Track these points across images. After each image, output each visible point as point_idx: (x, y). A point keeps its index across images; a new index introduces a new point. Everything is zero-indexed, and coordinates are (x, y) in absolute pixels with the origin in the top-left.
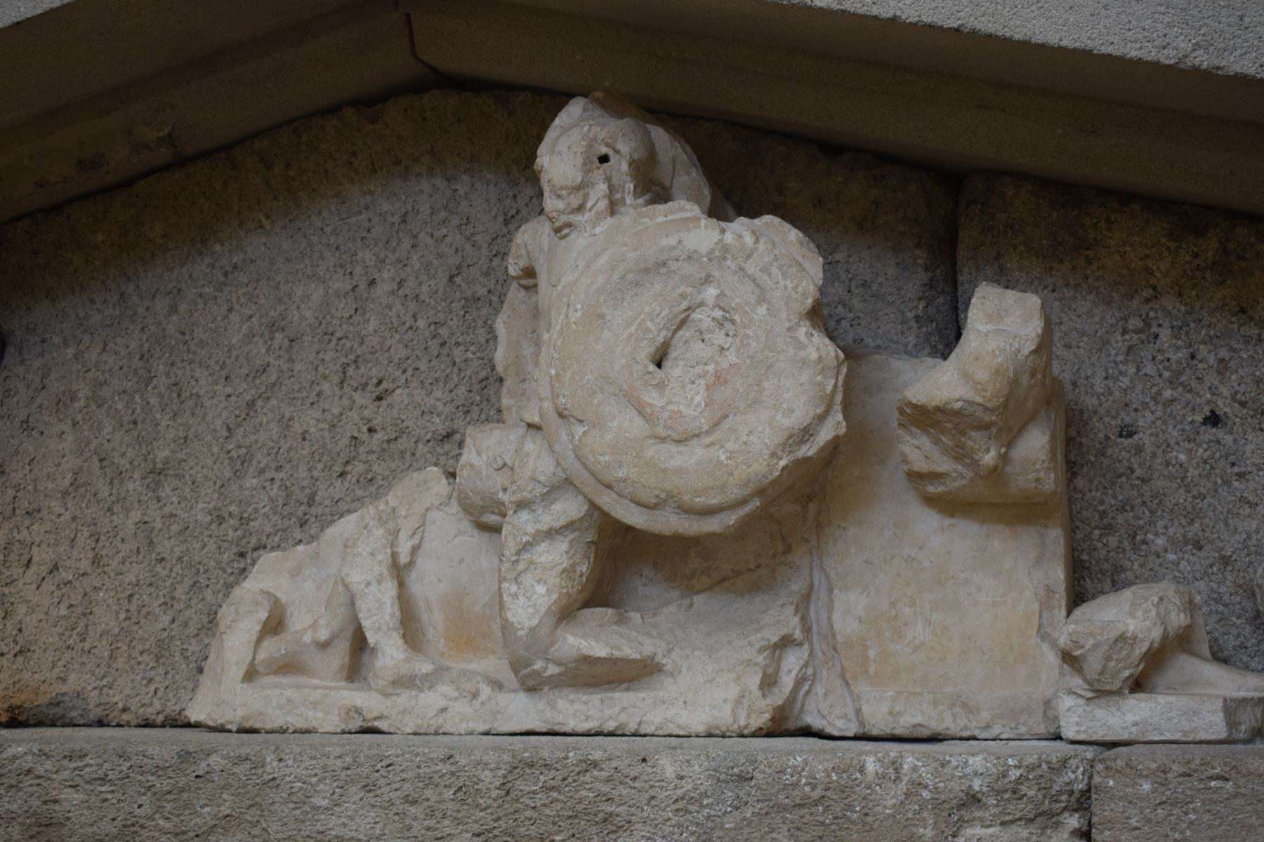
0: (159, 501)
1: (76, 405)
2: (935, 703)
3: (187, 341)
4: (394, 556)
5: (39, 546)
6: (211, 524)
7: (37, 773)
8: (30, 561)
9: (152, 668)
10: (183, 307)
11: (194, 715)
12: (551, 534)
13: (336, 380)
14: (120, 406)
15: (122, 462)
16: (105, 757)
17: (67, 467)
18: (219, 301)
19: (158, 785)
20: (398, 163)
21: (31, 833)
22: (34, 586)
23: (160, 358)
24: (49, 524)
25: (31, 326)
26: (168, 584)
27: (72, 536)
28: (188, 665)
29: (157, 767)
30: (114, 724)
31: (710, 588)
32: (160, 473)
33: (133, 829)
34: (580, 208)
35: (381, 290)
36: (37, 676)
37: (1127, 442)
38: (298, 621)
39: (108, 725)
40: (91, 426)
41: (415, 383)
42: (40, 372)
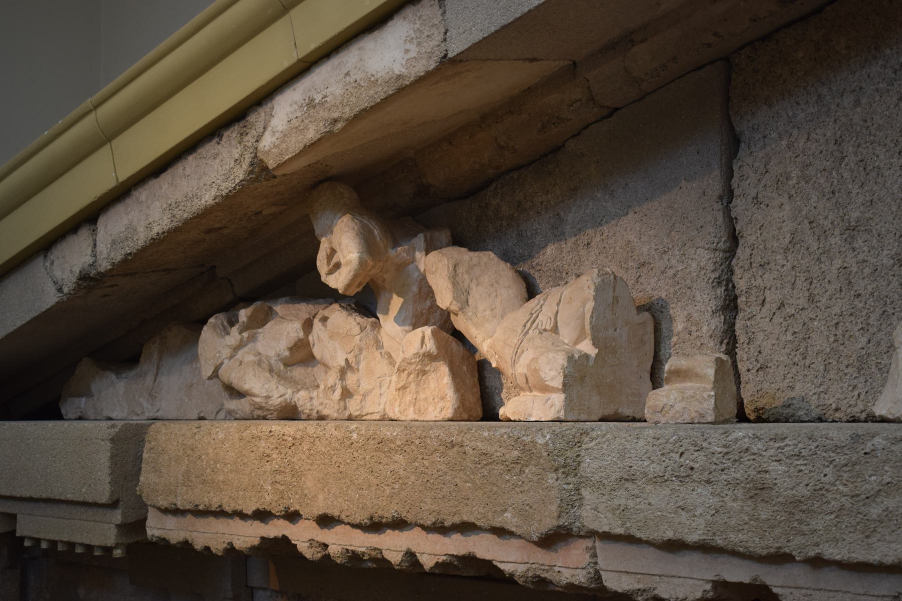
0: (854, 251)
1: (790, 183)
3: (868, 127)
5: (770, 289)
6: (893, 266)
7: (752, 451)
8: (764, 301)
9: (856, 377)
10: (864, 101)
11: (880, 410)
14: (822, 181)
15: (826, 223)
16: (799, 439)
17: (786, 229)
18: (891, 93)
19: (837, 460)
21: (751, 494)
22: (768, 319)
23: (849, 142)
24: (776, 273)
25: (756, 127)
26: (864, 313)
27: (793, 280)
28: (882, 375)
29: (836, 446)
30: (830, 420)
32: (853, 230)
33: (821, 492)
36: (773, 385)
39: (826, 421)
40: (802, 197)
42: (764, 160)
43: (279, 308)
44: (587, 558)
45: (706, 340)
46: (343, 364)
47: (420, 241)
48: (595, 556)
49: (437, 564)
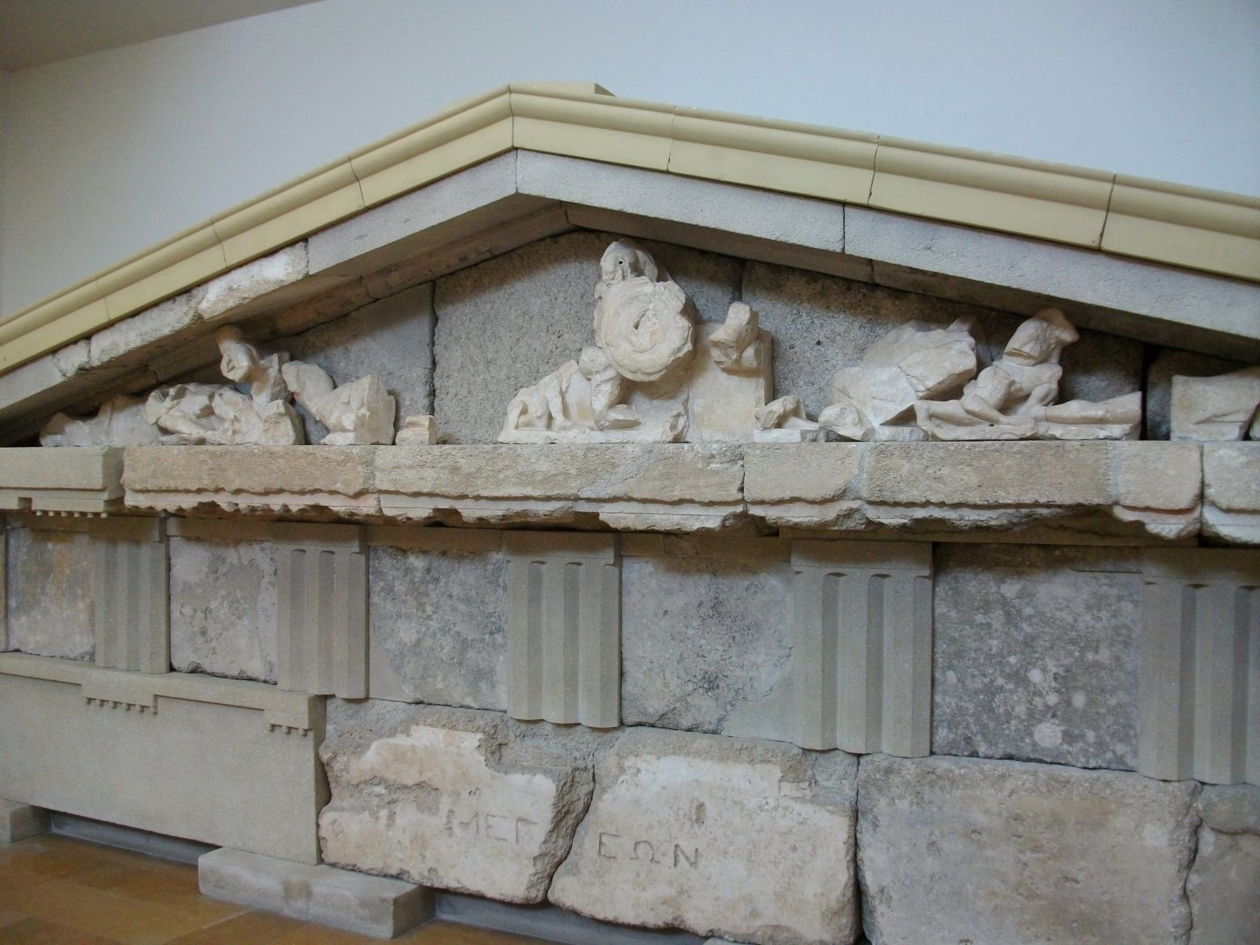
2: (723, 433)
4: (561, 389)
10: (495, 307)
11: (500, 440)
12: (606, 381)
13: (545, 331)
20: (564, 257)
31: (657, 398)
34: (613, 279)
35: (560, 300)
37: (791, 350)
38: (531, 410)
41: (570, 332)
43: (191, 387)
44: (376, 503)
46: (233, 417)
48: (380, 501)
49: (300, 510)
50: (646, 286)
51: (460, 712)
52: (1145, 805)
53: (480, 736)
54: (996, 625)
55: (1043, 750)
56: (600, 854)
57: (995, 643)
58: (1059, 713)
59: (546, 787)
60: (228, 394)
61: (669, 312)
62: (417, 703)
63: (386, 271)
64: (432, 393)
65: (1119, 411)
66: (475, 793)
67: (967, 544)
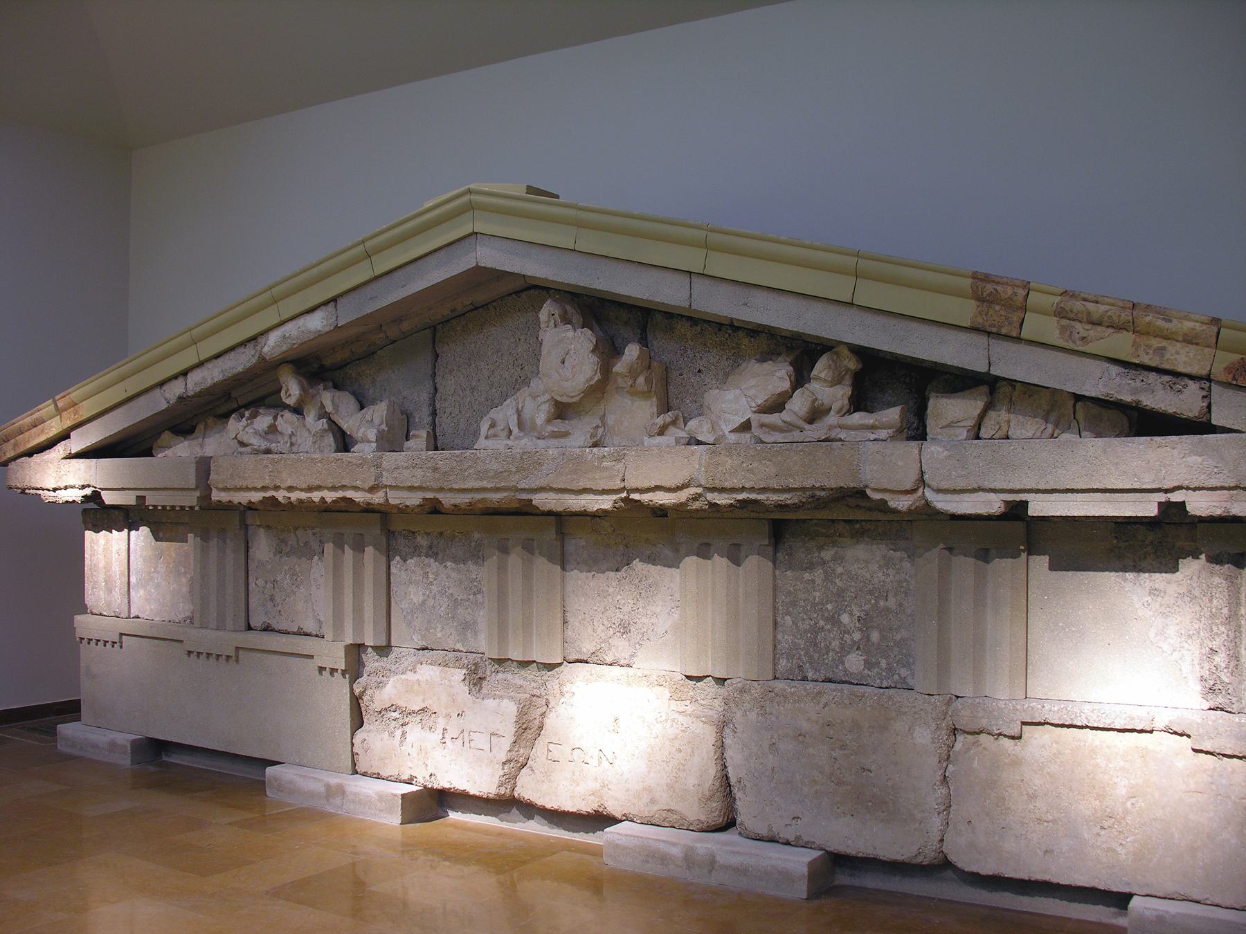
2: (628, 440)
13: (512, 364)
45: (426, 425)
46: (290, 433)
47: (321, 386)
50: (568, 333)
51: (451, 654)
52: (915, 713)
53: (464, 671)
54: (818, 581)
55: (851, 674)
56: (547, 758)
57: (818, 594)
58: (861, 646)
59: (510, 708)
60: (288, 415)
61: (584, 351)
62: (423, 649)
63: (400, 320)
64: (434, 413)
65: (884, 419)
66: (462, 715)
67: (797, 520)
